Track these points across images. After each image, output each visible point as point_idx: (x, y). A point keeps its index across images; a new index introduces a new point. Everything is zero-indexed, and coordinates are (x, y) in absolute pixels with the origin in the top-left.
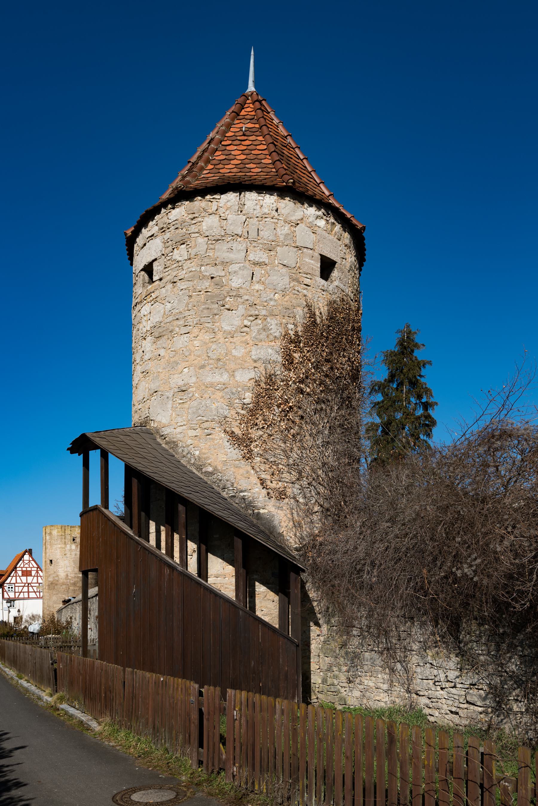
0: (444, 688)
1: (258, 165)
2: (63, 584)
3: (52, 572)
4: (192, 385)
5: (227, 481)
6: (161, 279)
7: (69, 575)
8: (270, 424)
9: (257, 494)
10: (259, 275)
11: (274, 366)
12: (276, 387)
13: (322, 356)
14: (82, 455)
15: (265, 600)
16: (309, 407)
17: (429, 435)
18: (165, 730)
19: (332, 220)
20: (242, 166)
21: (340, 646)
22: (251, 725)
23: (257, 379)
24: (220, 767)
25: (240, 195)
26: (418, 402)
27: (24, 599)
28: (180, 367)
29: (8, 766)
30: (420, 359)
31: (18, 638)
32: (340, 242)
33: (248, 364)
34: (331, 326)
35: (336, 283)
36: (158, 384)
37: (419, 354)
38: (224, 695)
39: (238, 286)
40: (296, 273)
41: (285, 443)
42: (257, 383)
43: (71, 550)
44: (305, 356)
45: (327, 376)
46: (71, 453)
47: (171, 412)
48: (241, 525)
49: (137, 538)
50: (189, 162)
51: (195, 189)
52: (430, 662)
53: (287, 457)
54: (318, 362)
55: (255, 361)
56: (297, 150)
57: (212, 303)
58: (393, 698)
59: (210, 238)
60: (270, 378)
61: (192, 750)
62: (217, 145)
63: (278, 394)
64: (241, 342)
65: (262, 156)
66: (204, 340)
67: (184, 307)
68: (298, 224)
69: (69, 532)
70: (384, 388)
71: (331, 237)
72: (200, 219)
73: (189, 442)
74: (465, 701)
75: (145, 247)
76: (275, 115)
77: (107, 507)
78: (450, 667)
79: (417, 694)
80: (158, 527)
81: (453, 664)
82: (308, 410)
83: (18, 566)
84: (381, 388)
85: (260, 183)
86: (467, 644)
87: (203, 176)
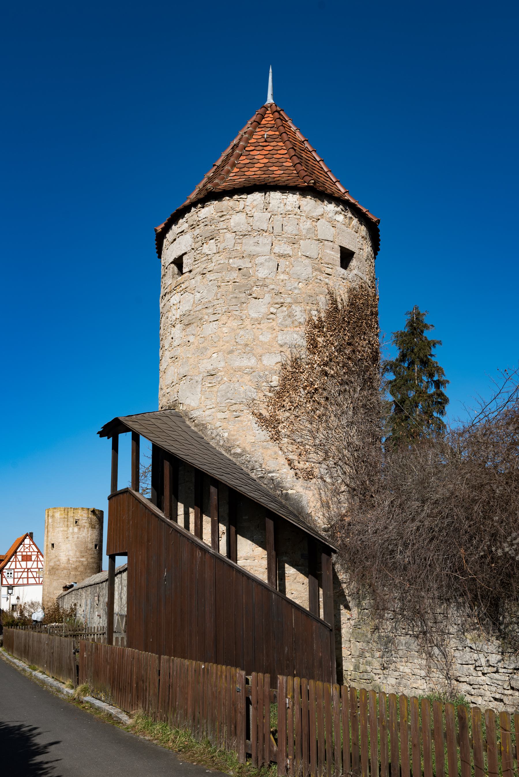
0: (486, 674)
1: (280, 168)
2: (64, 569)
3: (54, 557)
4: (221, 369)
5: (256, 462)
6: (190, 271)
7: (70, 559)
8: (297, 406)
9: (285, 475)
10: (284, 266)
11: (300, 350)
12: (301, 370)
13: (344, 340)
14: (111, 438)
15: (295, 583)
16: (333, 389)
17: (442, 413)
18: (206, 722)
19: (350, 215)
20: (265, 169)
21: (372, 630)
22: (306, 715)
23: (284, 362)
24: (271, 759)
25: (265, 194)
26: (430, 380)
27: (23, 585)
28: (209, 353)
29: (47, 763)
30: (429, 339)
31: (23, 627)
32: (357, 235)
33: (275, 349)
34: (352, 312)
35: (355, 272)
36: (187, 369)
37: (429, 335)
38: (273, 684)
39: (264, 277)
40: (318, 265)
41: (311, 424)
42: (284, 366)
43: (73, 533)
44: (328, 340)
45: (349, 358)
46: (101, 436)
47: (200, 395)
48: (272, 506)
49: (168, 520)
50: (214, 165)
51: (224, 190)
52: (469, 645)
53: (313, 437)
54: (341, 346)
55: (281, 346)
56: (314, 154)
57: (240, 292)
58: (432, 685)
59: (237, 233)
60: (296, 362)
61: (238, 742)
62: (241, 150)
63: (304, 376)
64: (268, 328)
65: (284, 160)
66: (232, 327)
67: (213, 296)
68: (319, 219)
69: (72, 515)
70: (396, 368)
71: (349, 230)
72: (228, 217)
73: (218, 424)
74: (509, 688)
75: (175, 242)
76: (292, 123)
77: (137, 490)
78: (491, 650)
79: (457, 681)
80: (186, 509)
81: (494, 647)
82: (333, 391)
83: (18, 550)
84: (393, 367)
85: (284, 184)
86: (508, 626)
87: (229, 178)
